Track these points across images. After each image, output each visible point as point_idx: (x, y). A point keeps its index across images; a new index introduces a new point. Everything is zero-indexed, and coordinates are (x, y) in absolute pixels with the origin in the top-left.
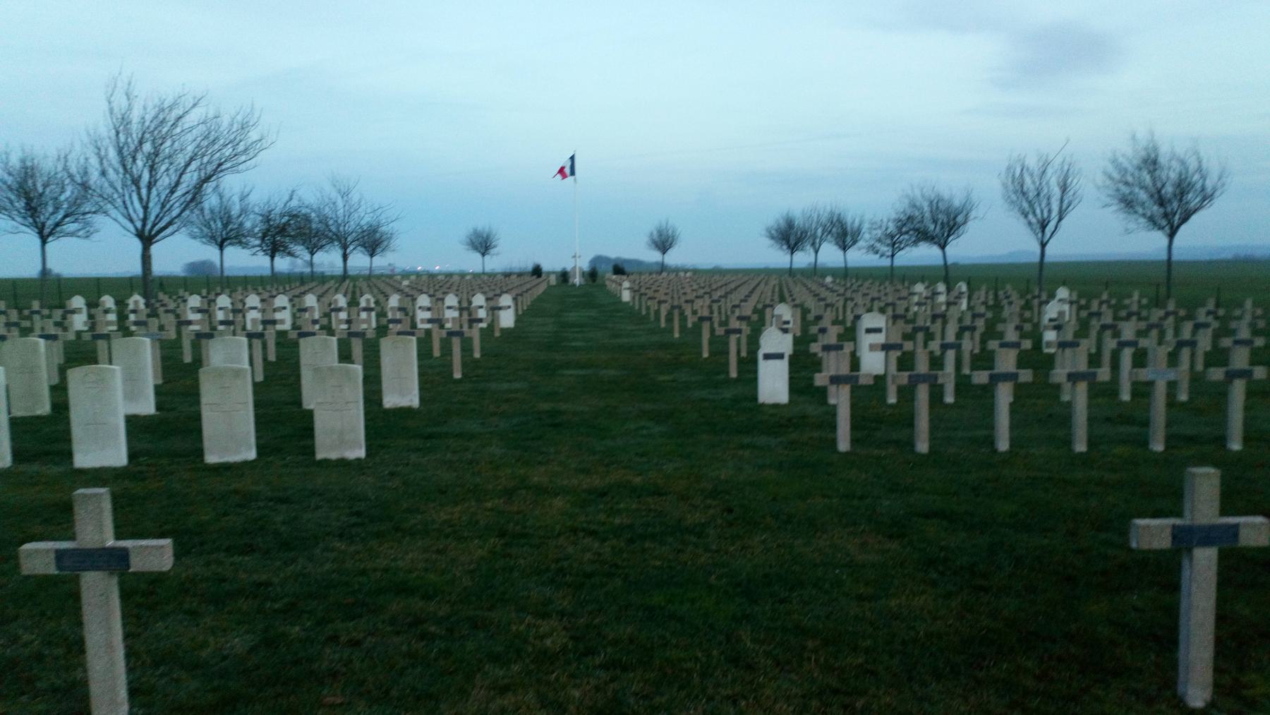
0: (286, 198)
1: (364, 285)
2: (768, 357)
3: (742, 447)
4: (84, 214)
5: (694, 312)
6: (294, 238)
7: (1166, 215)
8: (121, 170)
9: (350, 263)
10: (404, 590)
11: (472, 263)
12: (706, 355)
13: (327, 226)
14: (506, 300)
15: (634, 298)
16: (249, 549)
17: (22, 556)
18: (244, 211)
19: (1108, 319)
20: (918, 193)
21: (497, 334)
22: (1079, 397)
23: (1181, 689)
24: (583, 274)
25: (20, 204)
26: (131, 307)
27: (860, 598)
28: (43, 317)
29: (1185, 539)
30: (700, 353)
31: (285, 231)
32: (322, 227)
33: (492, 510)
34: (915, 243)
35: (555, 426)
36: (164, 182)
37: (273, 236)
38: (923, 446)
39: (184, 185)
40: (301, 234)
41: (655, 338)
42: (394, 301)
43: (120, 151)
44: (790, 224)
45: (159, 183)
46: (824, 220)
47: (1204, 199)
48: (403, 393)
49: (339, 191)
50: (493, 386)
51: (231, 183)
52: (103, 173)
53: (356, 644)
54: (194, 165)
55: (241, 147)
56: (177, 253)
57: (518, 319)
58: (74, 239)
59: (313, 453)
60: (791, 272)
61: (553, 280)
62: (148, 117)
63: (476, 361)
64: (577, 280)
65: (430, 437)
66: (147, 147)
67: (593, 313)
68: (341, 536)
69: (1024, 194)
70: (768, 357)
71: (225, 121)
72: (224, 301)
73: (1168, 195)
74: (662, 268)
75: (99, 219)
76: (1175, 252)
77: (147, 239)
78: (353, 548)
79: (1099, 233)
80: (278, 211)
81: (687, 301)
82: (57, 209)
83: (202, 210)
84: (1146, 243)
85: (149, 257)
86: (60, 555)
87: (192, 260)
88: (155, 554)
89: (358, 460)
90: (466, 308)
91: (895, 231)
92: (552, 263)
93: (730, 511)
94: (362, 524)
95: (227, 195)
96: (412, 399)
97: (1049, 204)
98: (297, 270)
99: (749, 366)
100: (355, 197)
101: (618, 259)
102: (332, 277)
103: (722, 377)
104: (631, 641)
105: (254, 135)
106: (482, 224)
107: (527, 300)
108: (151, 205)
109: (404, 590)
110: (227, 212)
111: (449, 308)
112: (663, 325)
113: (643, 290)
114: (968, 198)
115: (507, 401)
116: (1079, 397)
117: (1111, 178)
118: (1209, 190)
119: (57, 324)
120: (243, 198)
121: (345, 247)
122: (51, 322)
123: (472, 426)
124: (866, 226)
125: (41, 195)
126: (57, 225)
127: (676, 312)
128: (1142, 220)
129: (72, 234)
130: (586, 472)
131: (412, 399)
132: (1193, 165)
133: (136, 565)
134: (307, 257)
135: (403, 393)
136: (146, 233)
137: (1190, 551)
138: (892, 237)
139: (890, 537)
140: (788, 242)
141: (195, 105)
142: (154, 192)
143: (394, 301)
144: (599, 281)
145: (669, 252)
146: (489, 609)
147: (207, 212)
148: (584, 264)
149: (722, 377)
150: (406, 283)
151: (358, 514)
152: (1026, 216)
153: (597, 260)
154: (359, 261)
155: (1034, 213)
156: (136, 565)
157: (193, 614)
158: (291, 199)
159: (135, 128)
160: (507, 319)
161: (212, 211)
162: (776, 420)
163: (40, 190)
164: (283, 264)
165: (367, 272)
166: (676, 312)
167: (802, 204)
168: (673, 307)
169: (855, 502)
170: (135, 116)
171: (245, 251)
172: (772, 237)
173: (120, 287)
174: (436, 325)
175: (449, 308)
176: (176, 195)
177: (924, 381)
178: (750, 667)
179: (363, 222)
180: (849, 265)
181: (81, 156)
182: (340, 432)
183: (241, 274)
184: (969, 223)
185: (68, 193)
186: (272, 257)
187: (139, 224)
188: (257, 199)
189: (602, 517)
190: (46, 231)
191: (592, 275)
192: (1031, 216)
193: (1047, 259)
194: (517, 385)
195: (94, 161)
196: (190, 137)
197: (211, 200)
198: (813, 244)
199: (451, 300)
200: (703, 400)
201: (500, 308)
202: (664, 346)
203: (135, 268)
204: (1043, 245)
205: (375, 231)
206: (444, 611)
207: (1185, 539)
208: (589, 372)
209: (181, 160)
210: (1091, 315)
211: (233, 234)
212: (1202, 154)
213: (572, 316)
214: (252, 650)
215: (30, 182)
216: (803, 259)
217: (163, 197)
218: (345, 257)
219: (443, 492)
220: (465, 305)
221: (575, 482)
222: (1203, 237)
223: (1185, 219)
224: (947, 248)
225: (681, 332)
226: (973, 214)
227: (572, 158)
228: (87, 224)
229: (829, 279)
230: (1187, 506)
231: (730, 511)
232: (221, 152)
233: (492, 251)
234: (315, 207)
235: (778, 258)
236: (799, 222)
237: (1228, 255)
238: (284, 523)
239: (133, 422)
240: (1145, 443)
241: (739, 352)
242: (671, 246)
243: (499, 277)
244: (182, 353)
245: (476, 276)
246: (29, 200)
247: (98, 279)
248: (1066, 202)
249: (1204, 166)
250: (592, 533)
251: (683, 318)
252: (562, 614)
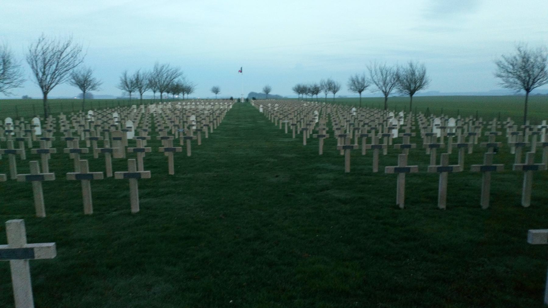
11: (213, 96)
22: (170, 156)
57: (233, 106)
61: (236, 101)
64: (243, 101)
74: (361, 98)
84: (357, 95)
86: (125, 174)
88: (46, 250)
92: (236, 96)
100: (186, 79)
106: (216, 85)
116: (170, 156)
133: (177, 151)
148: (246, 96)
160: (231, 107)
167: (309, 81)
191: (247, 100)
218: (161, 96)
235: (295, 95)
237: (115, 98)
241: (214, 128)
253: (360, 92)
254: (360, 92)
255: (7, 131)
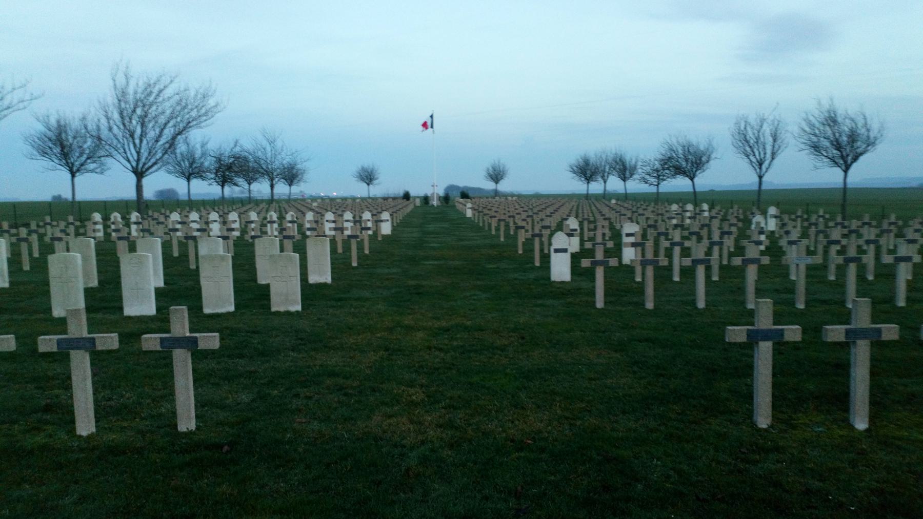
0: (232, 145)
1: (285, 205)
2: (557, 251)
3: (537, 306)
4: (100, 157)
5: (515, 223)
6: (237, 174)
7: (842, 157)
8: (122, 127)
9: (276, 191)
10: (333, 374)
11: (360, 190)
12: (520, 252)
13: (260, 165)
14: (385, 216)
15: (474, 215)
16: (241, 356)
17: (143, 340)
18: (204, 154)
19: (821, 227)
20: (674, 140)
21: (380, 239)
23: (755, 418)
24: (439, 198)
25: (57, 150)
26: (112, 220)
27: (591, 379)
28: (53, 226)
29: (755, 337)
30: (517, 251)
31: (232, 168)
32: (256, 165)
33: (380, 338)
34: (674, 176)
35: (418, 294)
36: (152, 134)
37: (223, 172)
38: (650, 305)
39: (164, 137)
40: (241, 171)
41: (487, 241)
42: (310, 216)
43: (121, 114)
44: (587, 162)
45: (148, 136)
46: (610, 159)
47: (868, 145)
48: (321, 274)
49: (268, 140)
50: (379, 271)
51: (196, 136)
52: (110, 129)
53: (310, 398)
54: (171, 124)
55: (203, 111)
56: (159, 182)
57: (394, 229)
58: (94, 175)
59: (270, 308)
60: (587, 196)
62: (140, 90)
63: (366, 255)
65: (340, 300)
66: (139, 111)
67: (446, 225)
68: (293, 351)
69: (747, 142)
70: (557, 251)
71: (192, 93)
72: (194, 216)
73: (842, 143)
74: (496, 193)
75: (109, 161)
76: (192, 192)
77: (140, 174)
78: (301, 356)
79: (799, 169)
80: (227, 154)
81: (510, 217)
82: (81, 154)
83: (175, 154)
84: (828, 176)
85: (141, 186)
86: (162, 340)
87: (161, 188)
89: (297, 312)
90: (357, 221)
91: (660, 167)
92: (417, 191)
93: (523, 338)
94: (304, 344)
95: (192, 144)
96: (327, 278)
97: (764, 149)
98: (235, 196)
99: (546, 258)
100: (279, 144)
101: (465, 187)
102: (262, 201)
103: (530, 265)
104: (459, 397)
105: (211, 102)
106: (367, 163)
107: (400, 216)
108: (142, 151)
109: (333, 374)
110: (192, 155)
111: (347, 221)
112: (493, 232)
113: (480, 209)
114: (710, 144)
115: (387, 279)
117: (804, 131)
118: (872, 140)
119: (62, 231)
120: (203, 145)
121: (272, 180)
122: (58, 229)
123: (367, 294)
124: (640, 163)
125: (71, 144)
126: (82, 165)
127: (502, 224)
128: (827, 160)
129: (92, 171)
130: (438, 319)
131: (327, 278)
132: (860, 123)
134: (246, 186)
135: (321, 274)
136: (139, 170)
137: (757, 343)
138: (657, 171)
139: (616, 351)
140: (585, 176)
141: (171, 81)
142: (145, 142)
143: (310, 216)
144: (451, 203)
145: (501, 182)
146: (382, 383)
147: (179, 155)
148: (441, 193)
149: (530, 265)
150: (315, 204)
151: (302, 339)
152: (747, 156)
153: (451, 188)
154: (282, 189)
155: (754, 155)
156: (202, 346)
157: (218, 384)
158: (235, 146)
159: (131, 98)
160: (386, 229)
161: (182, 154)
162: (562, 290)
163: (71, 140)
164: (228, 191)
165: (286, 197)
166: (502, 224)
167: (596, 147)
168: (499, 220)
169: (600, 334)
170: (131, 90)
171: (205, 182)
172: (574, 172)
173: (124, 207)
174: (339, 232)
175: (347, 221)
176: (160, 143)
177: (650, 264)
178: (523, 408)
179: (285, 162)
180: (193, 198)
181: (95, 117)
182: (286, 297)
183: (200, 198)
184: (711, 162)
185: (89, 143)
186: (223, 186)
187: (134, 164)
188: (212, 146)
189: (446, 341)
190: (75, 169)
191: (446, 199)
192: (752, 158)
193: (764, 187)
194: (394, 270)
195: (104, 121)
196: (167, 104)
197: (181, 148)
198: (603, 177)
199: (348, 216)
200: (516, 279)
201: (382, 221)
202: (493, 246)
203: (131, 194)
204: (760, 177)
205: (293, 168)
206: (356, 383)
207: (755, 337)
208: (442, 262)
209: (162, 120)
210: (811, 224)
211: (196, 170)
212: (867, 115)
213: (431, 227)
214: (253, 401)
215: (63, 135)
216: (596, 187)
217: (150, 145)
218: (272, 186)
219: (350, 329)
220: (357, 218)
221: (430, 324)
222: (867, 172)
223: (855, 159)
224: (696, 180)
225: (505, 238)
226: (713, 156)
227: (432, 117)
228: (102, 164)
229: (613, 201)
230: (756, 320)
231: (523, 338)
232: (187, 116)
233: (375, 182)
234: (251, 151)
235: (578, 186)
236: (593, 159)
237: (707, 189)
238: (259, 343)
239: (158, 291)
240: (793, 303)
241: (30, 254)
242: (502, 178)
243: (380, 200)
244: (171, 251)
245: (363, 199)
246: (63, 147)
247: (105, 202)
248: (777, 147)
249: (869, 122)
250: (441, 350)
251: (507, 226)
252: (422, 386)
253: (497, 182)
254: (497, 182)
255: (171, 230)
